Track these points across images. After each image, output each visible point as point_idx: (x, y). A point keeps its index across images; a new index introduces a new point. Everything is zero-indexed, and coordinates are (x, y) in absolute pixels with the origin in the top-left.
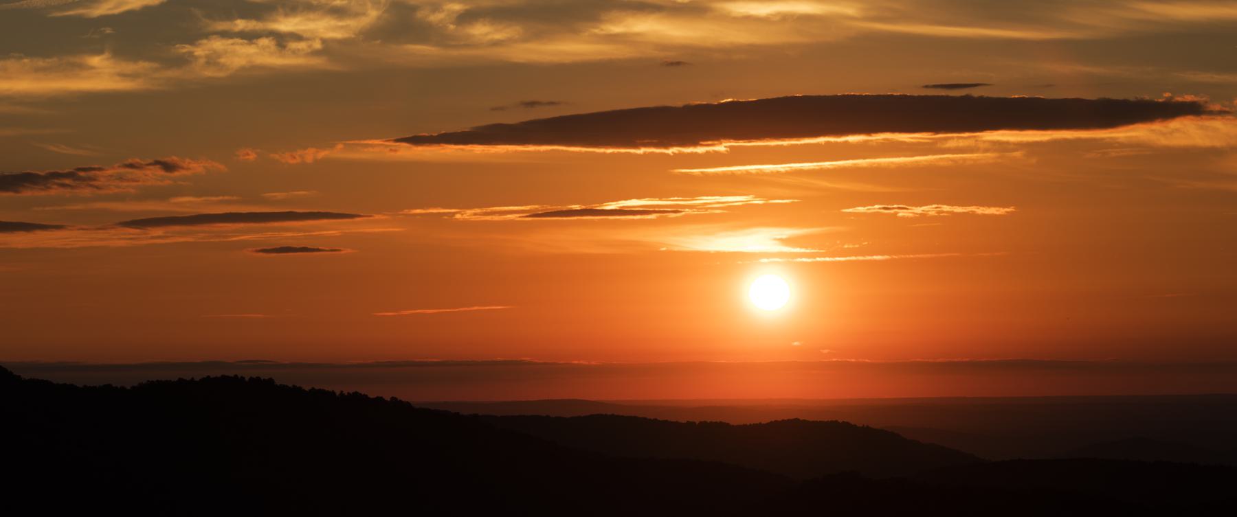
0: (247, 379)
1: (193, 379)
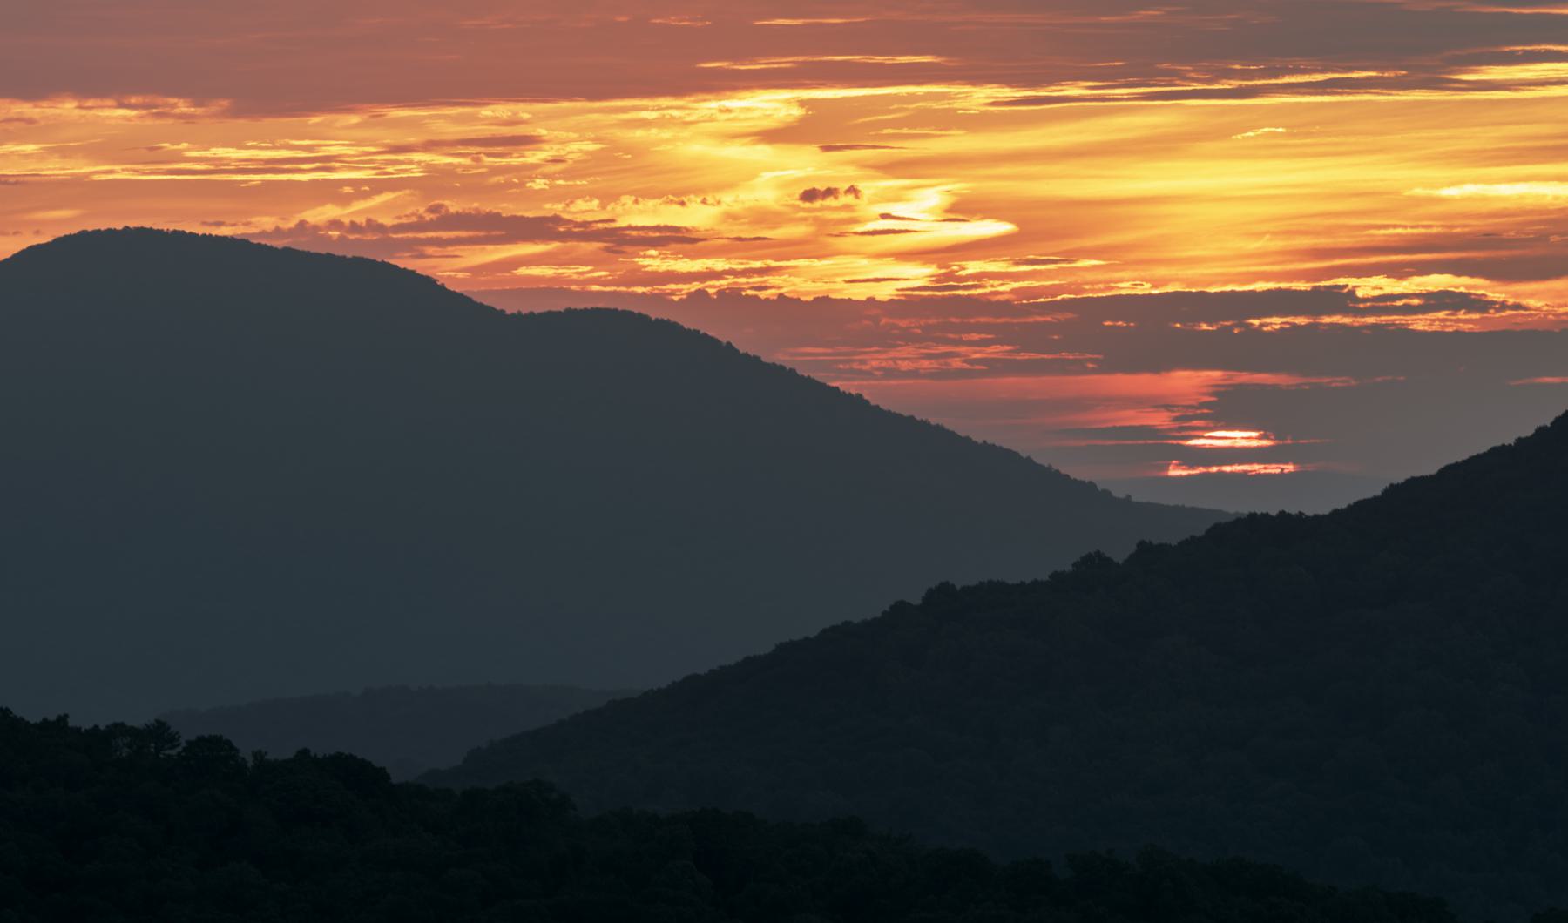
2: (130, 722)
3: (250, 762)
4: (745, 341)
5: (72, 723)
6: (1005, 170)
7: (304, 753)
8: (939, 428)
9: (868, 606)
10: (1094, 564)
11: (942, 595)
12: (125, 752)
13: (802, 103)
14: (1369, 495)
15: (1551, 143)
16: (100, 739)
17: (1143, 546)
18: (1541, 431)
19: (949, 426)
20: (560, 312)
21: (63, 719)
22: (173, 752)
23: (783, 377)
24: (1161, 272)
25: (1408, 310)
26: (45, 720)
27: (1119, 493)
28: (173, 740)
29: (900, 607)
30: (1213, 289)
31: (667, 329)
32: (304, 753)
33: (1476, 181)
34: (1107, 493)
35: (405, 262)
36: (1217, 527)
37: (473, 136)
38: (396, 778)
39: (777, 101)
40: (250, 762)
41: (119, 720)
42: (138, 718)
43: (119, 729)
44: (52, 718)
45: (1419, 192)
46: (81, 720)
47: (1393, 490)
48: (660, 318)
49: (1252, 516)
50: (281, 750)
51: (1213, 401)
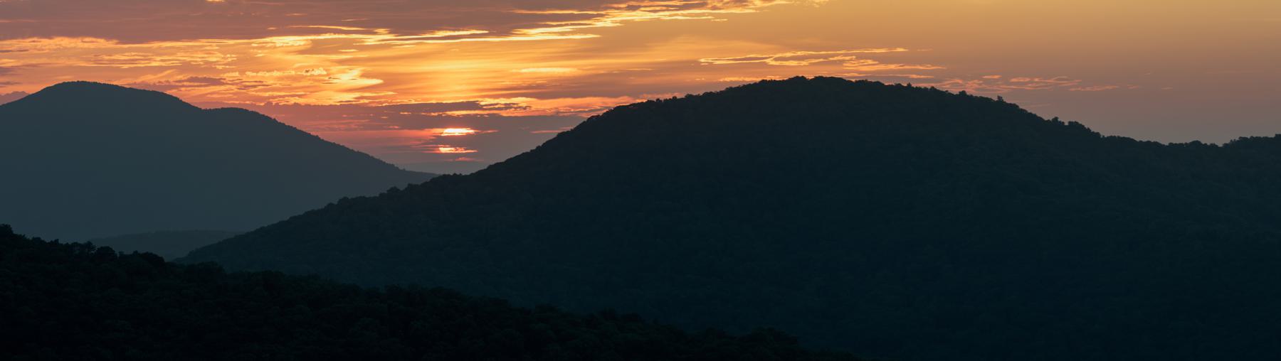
1: (1056, 118)
2: (79, 242)
3: (118, 255)
4: (280, 118)
5: (60, 242)
6: (377, 63)
7: (136, 252)
8: (343, 146)
9: (321, 205)
10: (394, 191)
11: (344, 201)
12: (77, 252)
13: (307, 40)
14: (482, 168)
15: (552, 55)
16: (69, 248)
17: (409, 185)
18: (538, 147)
19: (346, 146)
20: (1247, 138)
21: (57, 241)
22: (93, 252)
23: (292, 130)
24: (426, 96)
25: (500, 109)
26: (455, 174)
27: (401, 168)
28: (93, 248)
29: (331, 205)
30: (444, 102)
31: (255, 114)
32: (136, 252)
33: (534, 67)
34: (397, 168)
35: (168, 92)
36: (433, 179)
37: (496, 87)
38: (166, 260)
39: (517, 79)
40: (118, 255)
41: (75, 241)
42: (82, 241)
43: (75, 244)
44: (53, 240)
45: (514, 71)
46: (62, 241)
47: (490, 167)
48: (1113, 135)
49: (444, 175)
50: (128, 252)
51: (468, 135)
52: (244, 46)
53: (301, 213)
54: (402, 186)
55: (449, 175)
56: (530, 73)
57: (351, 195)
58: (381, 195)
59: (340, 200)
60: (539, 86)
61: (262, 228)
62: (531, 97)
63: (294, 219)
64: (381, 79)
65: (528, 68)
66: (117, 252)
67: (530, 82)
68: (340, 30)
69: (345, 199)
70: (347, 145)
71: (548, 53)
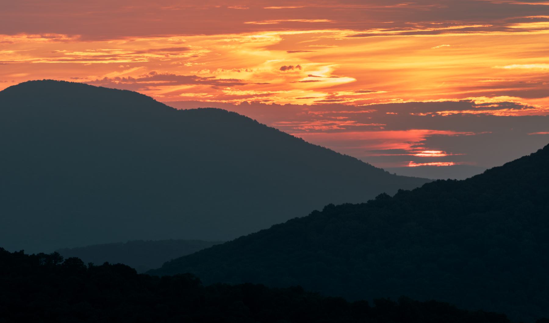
0: (29, 255)
2: (45, 253)
3: (88, 267)
4: (261, 119)
9: (304, 212)
10: (383, 197)
11: (330, 208)
15: (543, 50)
16: (35, 259)
17: (400, 190)
21: (22, 251)
22: (61, 263)
28: (61, 259)
29: (315, 213)
30: (425, 101)
31: (234, 115)
32: (106, 263)
33: (517, 63)
34: (388, 173)
35: (142, 92)
36: (426, 184)
37: (166, 47)
38: (139, 272)
40: (88, 267)
41: (41, 252)
42: (48, 251)
43: (42, 255)
44: (18, 251)
46: (28, 252)
47: (488, 172)
49: (439, 181)
52: (303, 50)
53: (284, 221)
54: (392, 193)
55: (443, 181)
56: (512, 70)
57: (337, 202)
58: (369, 201)
59: (326, 207)
60: (521, 84)
61: (242, 238)
62: (515, 96)
63: (276, 228)
64: (354, 77)
65: (512, 64)
66: (86, 264)
67: (518, 79)
68: (536, 18)
69: (331, 206)
70: (333, 148)
71: (538, 48)
